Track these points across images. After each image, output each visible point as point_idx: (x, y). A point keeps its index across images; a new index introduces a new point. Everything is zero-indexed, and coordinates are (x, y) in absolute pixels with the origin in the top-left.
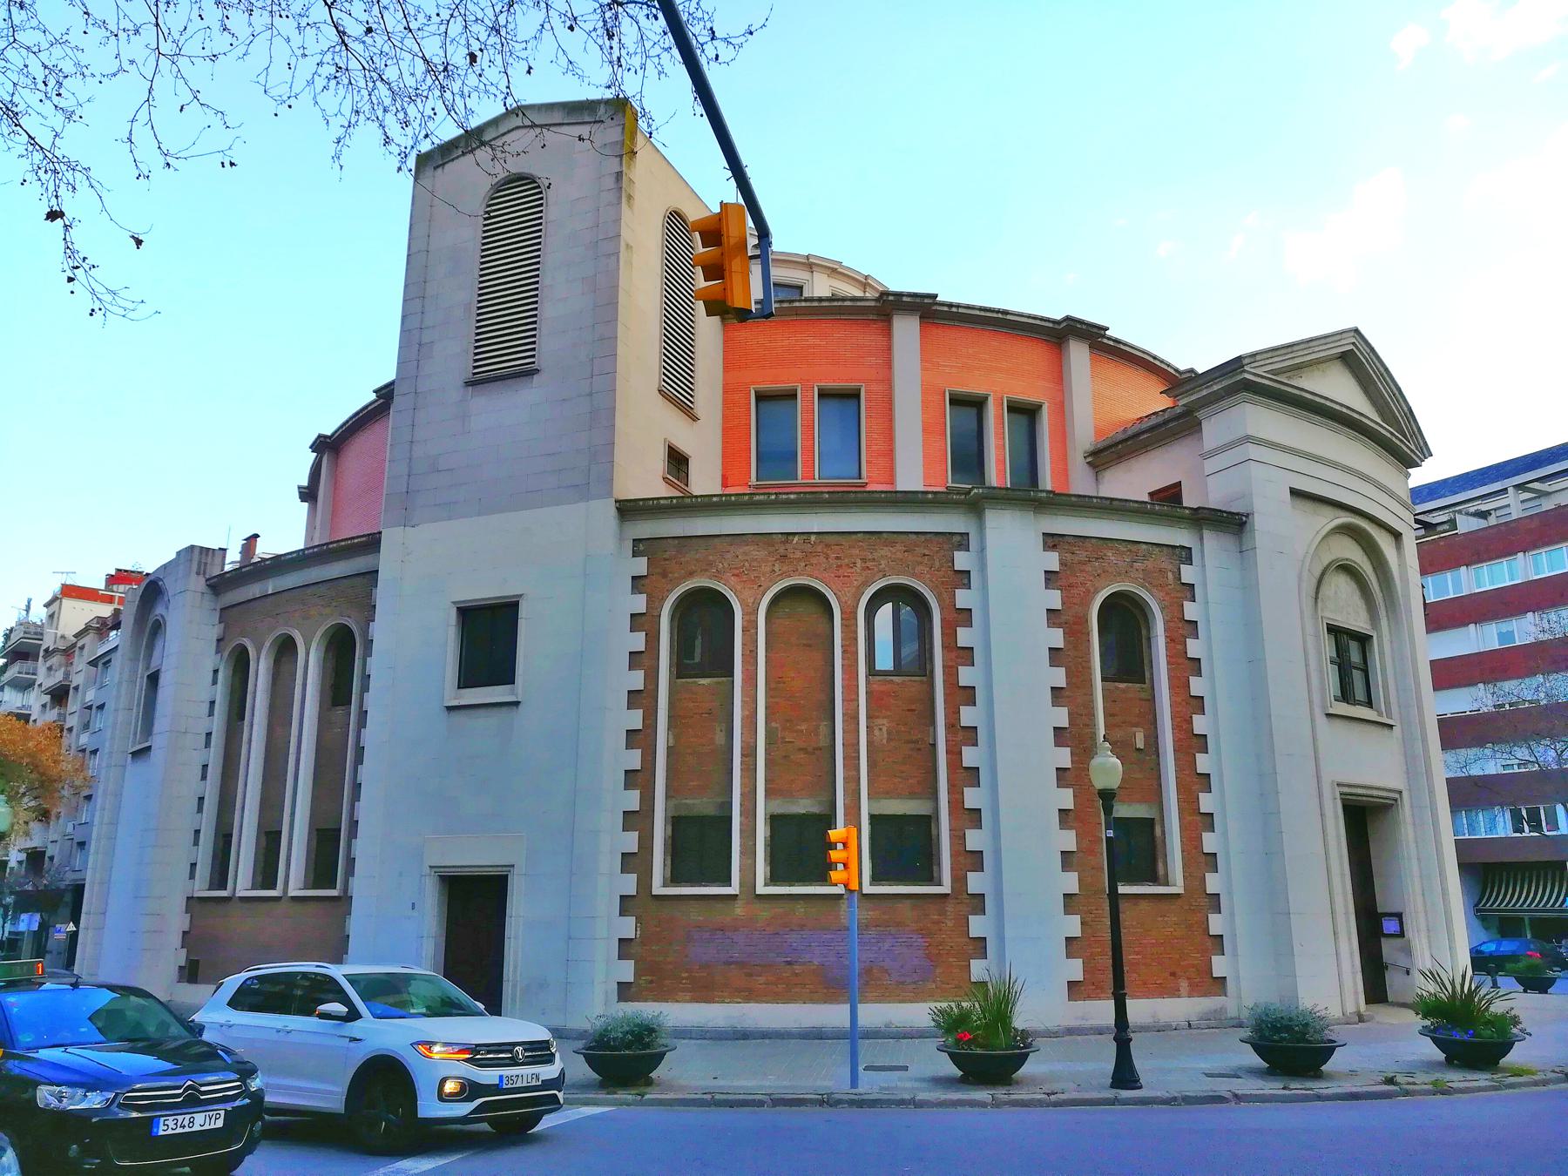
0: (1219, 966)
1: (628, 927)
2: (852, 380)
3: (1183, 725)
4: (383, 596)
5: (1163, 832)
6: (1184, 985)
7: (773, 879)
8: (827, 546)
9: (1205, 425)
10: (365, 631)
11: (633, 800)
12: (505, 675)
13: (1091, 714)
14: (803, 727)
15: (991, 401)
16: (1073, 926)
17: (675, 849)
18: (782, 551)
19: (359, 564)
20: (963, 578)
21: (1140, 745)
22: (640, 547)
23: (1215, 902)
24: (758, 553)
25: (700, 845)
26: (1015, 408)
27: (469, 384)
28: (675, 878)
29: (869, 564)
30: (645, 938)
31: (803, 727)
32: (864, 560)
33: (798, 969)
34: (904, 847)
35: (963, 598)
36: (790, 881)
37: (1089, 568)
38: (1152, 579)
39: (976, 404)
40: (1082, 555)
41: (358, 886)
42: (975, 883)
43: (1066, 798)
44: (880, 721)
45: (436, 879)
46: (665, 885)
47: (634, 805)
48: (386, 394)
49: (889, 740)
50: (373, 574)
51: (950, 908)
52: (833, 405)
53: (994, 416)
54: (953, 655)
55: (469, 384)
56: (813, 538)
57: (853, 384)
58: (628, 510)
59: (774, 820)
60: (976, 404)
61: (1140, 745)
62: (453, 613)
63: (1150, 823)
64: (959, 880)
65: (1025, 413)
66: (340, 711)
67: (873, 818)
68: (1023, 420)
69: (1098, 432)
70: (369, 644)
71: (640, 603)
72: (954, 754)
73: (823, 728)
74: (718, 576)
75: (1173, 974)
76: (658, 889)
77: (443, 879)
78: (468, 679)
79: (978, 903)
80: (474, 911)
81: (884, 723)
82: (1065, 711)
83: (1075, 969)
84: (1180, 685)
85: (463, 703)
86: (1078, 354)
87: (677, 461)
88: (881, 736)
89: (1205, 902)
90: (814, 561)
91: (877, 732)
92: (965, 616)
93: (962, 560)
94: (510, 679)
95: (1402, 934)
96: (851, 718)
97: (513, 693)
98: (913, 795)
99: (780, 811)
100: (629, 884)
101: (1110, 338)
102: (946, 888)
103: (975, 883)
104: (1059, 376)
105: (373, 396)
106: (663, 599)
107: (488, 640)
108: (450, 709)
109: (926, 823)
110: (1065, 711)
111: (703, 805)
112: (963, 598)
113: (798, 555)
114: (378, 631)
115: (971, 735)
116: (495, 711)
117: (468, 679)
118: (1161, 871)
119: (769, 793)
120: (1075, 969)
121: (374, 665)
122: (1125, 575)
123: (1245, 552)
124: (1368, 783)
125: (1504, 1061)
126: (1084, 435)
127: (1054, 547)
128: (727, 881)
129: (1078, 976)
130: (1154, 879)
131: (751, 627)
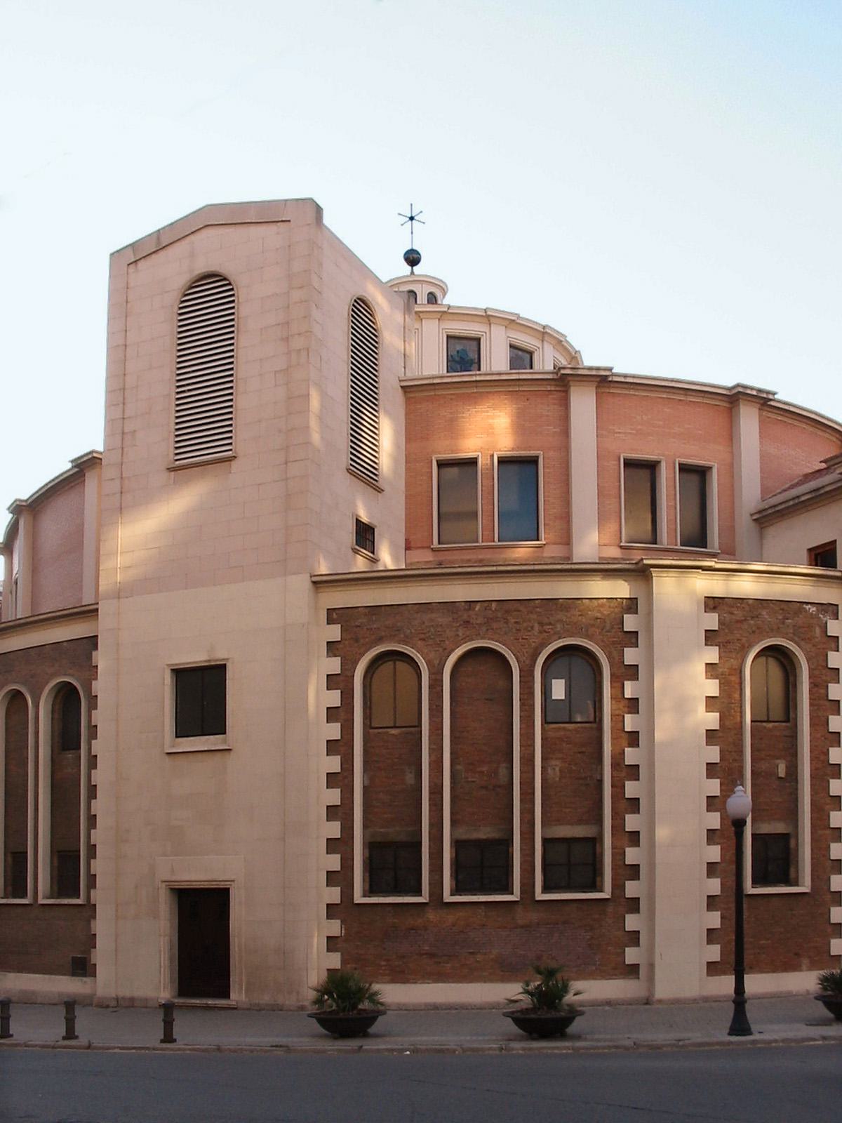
1: (335, 927)
2: (530, 448)
3: (820, 756)
4: (102, 659)
5: (797, 845)
6: (805, 961)
7: (457, 890)
8: (507, 612)
10: (88, 688)
11: (334, 829)
12: (218, 726)
13: (741, 752)
14: (485, 769)
15: (663, 465)
16: (714, 919)
18: (465, 617)
19: (77, 630)
20: (632, 638)
21: (782, 773)
22: (333, 616)
24: (443, 619)
25: (392, 863)
26: (685, 469)
27: (170, 470)
28: (371, 890)
30: (347, 938)
31: (485, 769)
32: (541, 624)
33: (479, 957)
34: (574, 863)
37: (745, 626)
38: (800, 635)
39: (651, 467)
40: (739, 614)
41: (97, 896)
42: (631, 889)
43: (714, 821)
44: (553, 762)
46: (364, 896)
47: (337, 834)
48: (85, 466)
51: (610, 909)
52: (514, 468)
53: (667, 479)
54: (621, 705)
55: (170, 470)
56: (494, 605)
57: (532, 453)
58: (319, 584)
59: (458, 844)
60: (651, 467)
62: (168, 679)
63: (785, 837)
64: (618, 887)
65: (696, 474)
66: (70, 755)
67: (545, 841)
68: (694, 478)
69: (765, 490)
70: (93, 701)
71: (334, 665)
72: (618, 787)
73: (503, 771)
74: (405, 642)
75: (796, 954)
76: (358, 898)
77: (172, 670)
78: (181, 732)
80: (202, 919)
81: (556, 764)
83: (714, 952)
85: (185, 750)
86: (749, 420)
87: (365, 535)
88: (554, 773)
89: (828, 897)
90: (495, 625)
91: (550, 771)
92: (632, 672)
93: (630, 623)
94: (222, 730)
96: (528, 761)
97: (225, 741)
98: (580, 822)
99: (464, 837)
100: (334, 895)
101: (779, 401)
102: (606, 894)
103: (631, 889)
104: (731, 436)
105: (11, 515)
106: (356, 662)
107: (200, 698)
108: (168, 753)
109: (594, 842)
111: (396, 833)
112: (630, 656)
114: (99, 687)
118: (792, 875)
119: (454, 823)
120: (714, 952)
121: (99, 717)
122: (776, 631)
125: (372, 1030)
126: (751, 494)
127: (714, 609)
129: (717, 958)
130: (787, 882)
131: (436, 684)
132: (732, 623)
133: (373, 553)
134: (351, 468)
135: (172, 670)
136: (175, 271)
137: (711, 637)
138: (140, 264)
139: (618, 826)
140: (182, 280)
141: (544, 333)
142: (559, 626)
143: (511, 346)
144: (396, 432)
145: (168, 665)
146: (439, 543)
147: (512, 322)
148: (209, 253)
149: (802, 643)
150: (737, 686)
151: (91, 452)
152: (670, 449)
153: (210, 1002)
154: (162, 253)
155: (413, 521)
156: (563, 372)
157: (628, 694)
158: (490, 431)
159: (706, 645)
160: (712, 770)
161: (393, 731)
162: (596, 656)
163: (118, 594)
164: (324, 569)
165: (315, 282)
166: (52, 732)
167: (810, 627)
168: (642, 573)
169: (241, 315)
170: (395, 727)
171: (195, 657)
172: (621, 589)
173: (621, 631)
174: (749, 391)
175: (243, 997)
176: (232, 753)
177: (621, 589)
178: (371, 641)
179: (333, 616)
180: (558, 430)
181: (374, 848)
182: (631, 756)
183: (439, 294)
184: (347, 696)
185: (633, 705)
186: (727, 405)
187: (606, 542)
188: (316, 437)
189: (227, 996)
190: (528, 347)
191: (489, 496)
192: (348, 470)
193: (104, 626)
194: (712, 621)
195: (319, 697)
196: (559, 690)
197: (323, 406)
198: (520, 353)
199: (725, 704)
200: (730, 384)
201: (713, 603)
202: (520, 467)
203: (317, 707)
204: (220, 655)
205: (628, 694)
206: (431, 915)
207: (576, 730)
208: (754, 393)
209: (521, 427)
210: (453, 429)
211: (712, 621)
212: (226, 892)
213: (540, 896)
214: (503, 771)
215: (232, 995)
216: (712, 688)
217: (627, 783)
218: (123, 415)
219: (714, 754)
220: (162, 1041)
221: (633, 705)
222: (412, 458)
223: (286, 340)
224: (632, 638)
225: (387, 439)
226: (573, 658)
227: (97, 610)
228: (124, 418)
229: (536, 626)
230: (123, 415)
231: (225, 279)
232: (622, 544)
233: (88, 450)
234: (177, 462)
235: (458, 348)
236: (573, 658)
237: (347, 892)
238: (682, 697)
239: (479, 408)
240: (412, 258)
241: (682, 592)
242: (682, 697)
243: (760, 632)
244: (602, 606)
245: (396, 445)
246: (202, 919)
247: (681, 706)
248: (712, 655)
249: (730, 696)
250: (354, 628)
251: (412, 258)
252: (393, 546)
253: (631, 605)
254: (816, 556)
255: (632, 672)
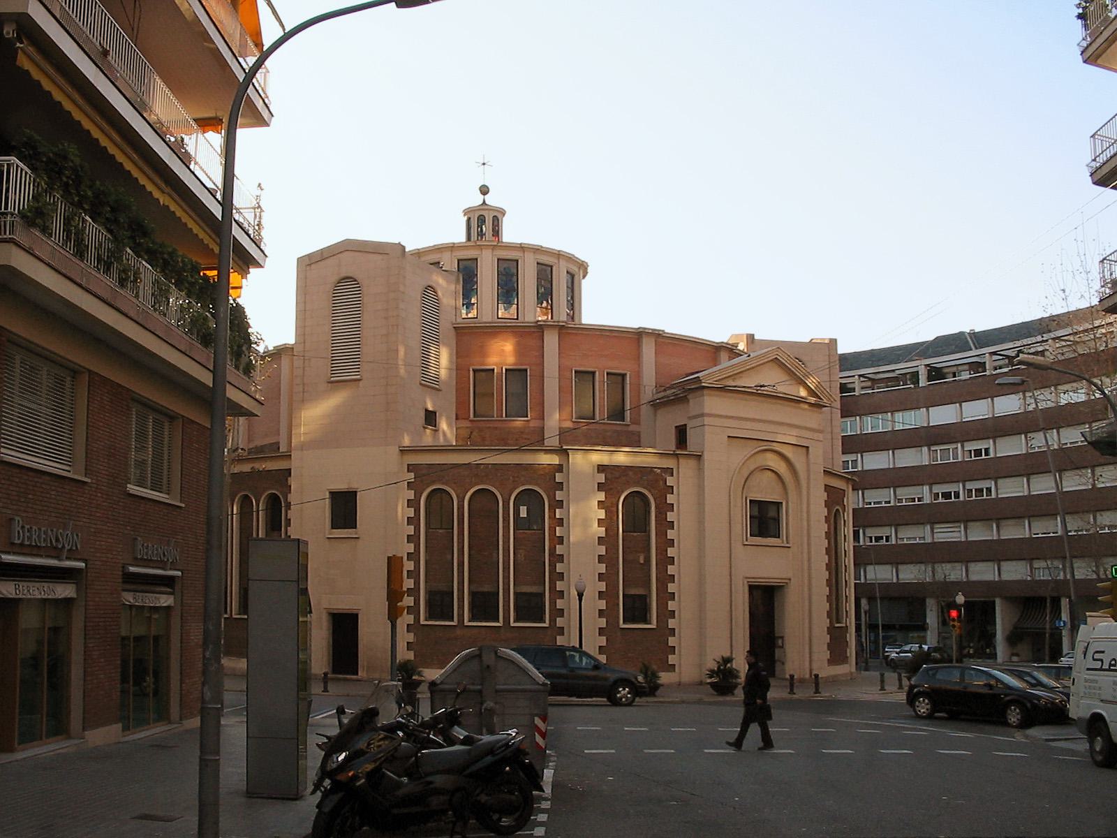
0: (672, 659)
3: (662, 552)
4: (293, 482)
9: (691, 401)
17: (429, 604)
18: (476, 472)
20: (560, 486)
21: (642, 562)
22: (410, 468)
23: (672, 632)
28: (431, 616)
29: (517, 479)
32: (513, 477)
35: (559, 495)
36: (634, 621)
45: (327, 614)
46: (470, 621)
49: (525, 560)
50: (288, 472)
56: (490, 466)
58: (404, 451)
59: (473, 594)
61: (642, 562)
64: (553, 621)
69: (658, 386)
70: (288, 506)
72: (553, 567)
73: (495, 555)
77: (330, 492)
78: (334, 525)
79: (672, 632)
81: (522, 552)
82: (604, 547)
84: (662, 534)
88: (521, 557)
92: (560, 504)
93: (559, 478)
95: (782, 647)
96: (507, 550)
97: (356, 534)
102: (653, 626)
107: (344, 508)
110: (604, 547)
112: (559, 495)
113: (483, 474)
114: (292, 498)
115: (561, 558)
116: (347, 540)
117: (334, 525)
122: (637, 484)
123: (700, 470)
124: (766, 576)
126: (649, 392)
128: (646, 620)
131: (461, 508)
132: (612, 478)
133: (435, 426)
134: (423, 382)
135: (330, 492)
136: (330, 273)
137: (600, 487)
138: (312, 266)
139: (553, 586)
140: (335, 278)
141: (559, 254)
142: (522, 479)
143: (538, 263)
144: (451, 355)
145: (328, 489)
146: (474, 417)
147: (537, 250)
148: (349, 266)
149: (652, 490)
150: (615, 513)
151: (285, 344)
152: (601, 365)
153: (348, 676)
154: (323, 262)
155: (461, 405)
156: (539, 323)
157: (557, 516)
158: (502, 354)
159: (598, 490)
160: (601, 559)
161: (441, 531)
162: (541, 498)
163: (303, 447)
164: (407, 441)
165: (402, 288)
166: (266, 521)
167: (657, 481)
168: (564, 453)
169: (365, 302)
170: (441, 529)
171: (341, 486)
172: (554, 460)
173: (553, 480)
174: (647, 331)
175: (365, 676)
176: (360, 540)
177: (554, 460)
178: (431, 485)
179: (410, 468)
180: (537, 354)
181: (431, 594)
182: (559, 550)
183: (499, 216)
184: (417, 511)
185: (560, 522)
186: (637, 337)
187: (564, 418)
188: (402, 371)
189: (357, 674)
190: (550, 264)
191: (500, 387)
192: (421, 384)
193: (295, 464)
194: (601, 478)
195: (403, 511)
196: (523, 512)
197: (406, 354)
198: (544, 267)
199: (605, 523)
200: (637, 327)
201: (601, 468)
202: (516, 374)
203: (403, 516)
204: (354, 486)
205: (557, 516)
206: (458, 632)
207: (531, 534)
208: (650, 331)
209: (520, 351)
210: (483, 353)
211: (601, 478)
212: (356, 616)
213: (466, 623)
214: (495, 555)
215: (360, 674)
216: (602, 514)
217: (557, 564)
218: (304, 348)
219: (602, 550)
220: (323, 691)
221: (560, 522)
222: (459, 368)
223: (386, 318)
224: (560, 486)
225: (443, 359)
226: (529, 497)
227: (290, 455)
228: (305, 326)
229: (511, 478)
230: (304, 348)
231: (355, 281)
232: (573, 420)
233: (284, 343)
234: (332, 379)
235: (505, 266)
236: (529, 497)
237: (417, 619)
238: (585, 519)
239: (496, 340)
240: (484, 190)
241: (586, 461)
242: (585, 519)
243: (628, 484)
244: (545, 468)
245: (450, 361)
246: (345, 626)
247: (586, 524)
248: (602, 496)
249: (611, 519)
250: (421, 475)
251: (484, 190)
252: (448, 418)
253: (560, 468)
254: (680, 431)
255: (560, 504)
